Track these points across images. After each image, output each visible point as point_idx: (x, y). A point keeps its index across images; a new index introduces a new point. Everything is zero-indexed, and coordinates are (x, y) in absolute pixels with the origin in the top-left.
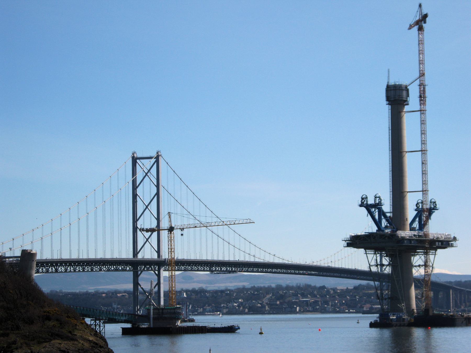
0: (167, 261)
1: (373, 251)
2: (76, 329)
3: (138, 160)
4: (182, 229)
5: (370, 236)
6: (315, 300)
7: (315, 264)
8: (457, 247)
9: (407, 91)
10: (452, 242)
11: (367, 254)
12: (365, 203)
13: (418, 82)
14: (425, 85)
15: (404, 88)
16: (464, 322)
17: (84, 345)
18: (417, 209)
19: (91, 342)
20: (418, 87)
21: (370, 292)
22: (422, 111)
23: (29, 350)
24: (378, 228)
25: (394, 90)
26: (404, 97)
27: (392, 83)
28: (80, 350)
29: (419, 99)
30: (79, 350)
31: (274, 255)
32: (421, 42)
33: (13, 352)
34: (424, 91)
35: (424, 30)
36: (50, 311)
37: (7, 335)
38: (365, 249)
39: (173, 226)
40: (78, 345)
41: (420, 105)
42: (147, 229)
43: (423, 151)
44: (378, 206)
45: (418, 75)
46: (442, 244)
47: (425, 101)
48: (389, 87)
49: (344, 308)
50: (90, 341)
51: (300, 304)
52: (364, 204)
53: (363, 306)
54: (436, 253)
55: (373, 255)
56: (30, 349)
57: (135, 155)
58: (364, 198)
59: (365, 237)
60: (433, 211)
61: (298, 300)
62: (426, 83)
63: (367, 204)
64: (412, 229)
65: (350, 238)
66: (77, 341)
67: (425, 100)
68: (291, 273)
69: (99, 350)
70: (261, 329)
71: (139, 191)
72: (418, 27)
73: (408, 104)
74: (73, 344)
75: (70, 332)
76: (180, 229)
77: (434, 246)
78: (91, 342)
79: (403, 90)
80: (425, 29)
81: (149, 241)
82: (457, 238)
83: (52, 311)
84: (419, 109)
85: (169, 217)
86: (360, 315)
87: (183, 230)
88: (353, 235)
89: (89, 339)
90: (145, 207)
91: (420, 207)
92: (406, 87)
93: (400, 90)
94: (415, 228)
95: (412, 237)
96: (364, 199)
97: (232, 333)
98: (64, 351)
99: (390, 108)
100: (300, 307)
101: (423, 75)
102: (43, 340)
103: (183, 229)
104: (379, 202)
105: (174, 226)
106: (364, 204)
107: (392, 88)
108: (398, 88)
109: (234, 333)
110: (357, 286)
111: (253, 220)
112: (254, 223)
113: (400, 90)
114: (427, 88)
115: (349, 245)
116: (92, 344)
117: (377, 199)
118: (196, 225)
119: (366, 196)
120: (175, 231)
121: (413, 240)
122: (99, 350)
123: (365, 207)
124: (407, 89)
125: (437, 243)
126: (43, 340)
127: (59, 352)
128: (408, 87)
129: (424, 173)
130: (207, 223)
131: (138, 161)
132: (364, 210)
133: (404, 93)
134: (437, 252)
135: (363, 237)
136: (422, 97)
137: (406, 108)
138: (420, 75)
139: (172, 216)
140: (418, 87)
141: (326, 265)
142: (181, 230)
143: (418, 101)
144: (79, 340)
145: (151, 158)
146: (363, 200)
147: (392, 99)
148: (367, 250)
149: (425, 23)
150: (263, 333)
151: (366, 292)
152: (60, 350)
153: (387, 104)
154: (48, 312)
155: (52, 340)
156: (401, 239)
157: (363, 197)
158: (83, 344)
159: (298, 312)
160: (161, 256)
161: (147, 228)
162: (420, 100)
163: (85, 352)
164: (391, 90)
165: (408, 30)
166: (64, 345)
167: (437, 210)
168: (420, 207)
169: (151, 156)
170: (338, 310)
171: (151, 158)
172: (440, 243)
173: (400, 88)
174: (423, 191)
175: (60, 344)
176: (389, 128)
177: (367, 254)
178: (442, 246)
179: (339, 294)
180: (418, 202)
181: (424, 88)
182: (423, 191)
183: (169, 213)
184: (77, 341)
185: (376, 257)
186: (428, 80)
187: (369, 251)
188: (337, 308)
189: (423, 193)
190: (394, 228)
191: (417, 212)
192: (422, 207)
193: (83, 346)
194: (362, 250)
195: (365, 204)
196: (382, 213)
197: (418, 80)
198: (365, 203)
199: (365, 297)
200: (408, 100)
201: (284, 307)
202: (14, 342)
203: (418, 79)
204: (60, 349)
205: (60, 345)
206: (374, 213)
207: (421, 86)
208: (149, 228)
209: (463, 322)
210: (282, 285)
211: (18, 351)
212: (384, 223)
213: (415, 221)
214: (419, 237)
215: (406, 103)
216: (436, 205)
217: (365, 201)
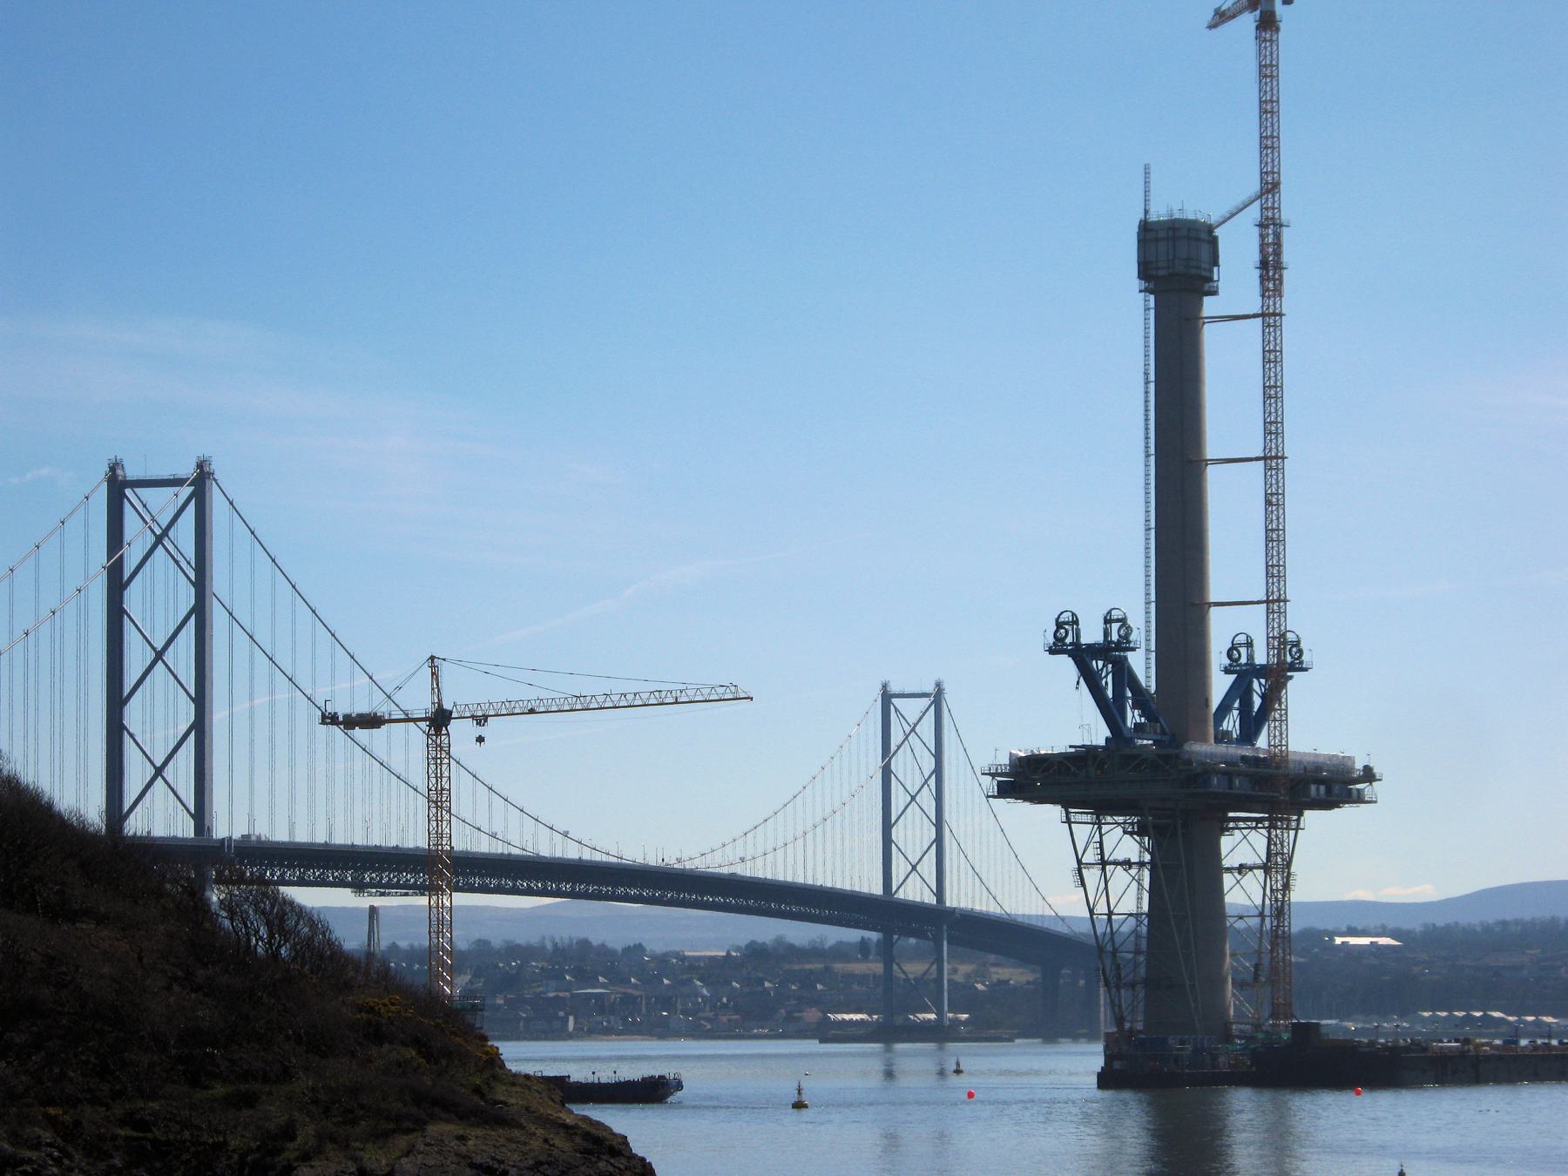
0: (230, 846)
1: (1078, 813)
2: (494, 1077)
3: (130, 490)
4: (481, 720)
5: (1083, 757)
6: (625, 993)
7: (689, 866)
8: (1376, 802)
9: (1213, 242)
11: (1072, 825)
12: (1069, 640)
13: (1254, 212)
14: (1281, 226)
15: (1204, 236)
17: (553, 1145)
18: (1230, 665)
19: (570, 1131)
20: (1255, 232)
21: (808, 966)
22: (1270, 317)
23: (350, 1163)
24: (1111, 732)
26: (1203, 266)
27: (1159, 213)
28: (541, 1163)
29: (1258, 273)
30: (539, 1163)
31: (565, 834)
32: (1267, 72)
33: (295, 1172)
34: (1278, 244)
35: (1278, 30)
36: (378, 1004)
37: (249, 1100)
38: (1066, 805)
39: (447, 706)
40: (530, 1144)
41: (1263, 296)
42: (347, 717)
43: (1272, 460)
44: (1113, 651)
45: (1254, 187)
46: (1329, 791)
47: (1281, 283)
48: (1152, 230)
49: (729, 1020)
50: (566, 1127)
51: (580, 1007)
52: (1065, 644)
53: (796, 1014)
54: (1302, 826)
56: (355, 1159)
57: (119, 472)
58: (1067, 623)
59: (1066, 762)
60: (1289, 674)
61: (568, 993)
63: (1076, 644)
64: (1220, 737)
65: (1010, 765)
66: (520, 1127)
67: (1281, 276)
68: (626, 898)
69: (615, 1167)
71: (133, 599)
72: (1258, 19)
73: (1214, 293)
74: (510, 1140)
75: (477, 1090)
76: (473, 717)
77: (1304, 799)
78: (576, 1134)
80: (1282, 26)
81: (165, 775)
83: (385, 1005)
84: (1257, 309)
85: (433, 674)
86: (812, 1046)
87: (486, 721)
88: (1022, 754)
89: (561, 1122)
90: (153, 654)
91: (1243, 660)
92: (1210, 229)
94: (1228, 733)
96: (1066, 625)
97: (655, 1106)
98: (489, 1170)
99: (1152, 304)
101: (1276, 185)
102: (391, 1126)
103: (486, 717)
104: (1119, 636)
105: (450, 708)
106: (1065, 641)
107: (1162, 234)
109: (663, 1106)
110: (619, 947)
111: (745, 688)
112: (752, 699)
114: (1286, 234)
115: (1005, 791)
116: (578, 1139)
117: (1115, 626)
118: (533, 704)
119: (1073, 614)
120: (454, 726)
121: (1239, 774)
122: (615, 1167)
123: (1071, 654)
124: (1211, 239)
125: (1313, 788)
126: (391, 1126)
127: (468, 1171)
128: (1217, 232)
130: (575, 699)
131: (128, 492)
132: (1066, 664)
133: (1205, 249)
134: (1302, 818)
135: (1060, 763)
136: (1270, 267)
137: (1210, 306)
138: (1262, 188)
139: (445, 670)
140: (1256, 231)
141: (725, 871)
142: (475, 722)
143: (1257, 281)
144: (525, 1124)
145: (176, 482)
146: (1062, 631)
147: (1161, 273)
148: (1070, 810)
150: (806, 1106)
151: (797, 967)
152: (472, 1166)
153: (1140, 291)
154: (371, 1010)
155: (425, 1123)
156: (1199, 770)
157: (1061, 620)
158: (546, 1141)
159: (571, 1033)
160: (206, 829)
161: (348, 711)
162: (1264, 279)
163: (563, 1172)
164: (1157, 240)
165: (1208, 30)
166: (481, 1143)
167: (1306, 670)
168: (1243, 660)
169: (176, 477)
170: (709, 1027)
171: (176, 482)
172: (1322, 788)
174: (1267, 602)
175: (462, 1138)
176: (1146, 374)
177: (1072, 825)
178: (1330, 798)
179: (701, 971)
180: (1237, 640)
181: (1278, 236)
182: (1267, 602)
183: (432, 658)
184: (520, 1127)
185: (1101, 836)
186: (1290, 205)
187: (1078, 815)
188: (703, 1022)
189: (1268, 609)
190: (1163, 732)
191: (1233, 677)
192: (1248, 660)
193: (547, 1147)
194: (1054, 812)
195: (1071, 644)
196: (1124, 675)
197: (1257, 204)
198: (1069, 640)
199: (795, 985)
200: (1215, 278)
201: (524, 1015)
202: (288, 1133)
203: (1257, 199)
204: (470, 1161)
205: (464, 1142)
206: (1103, 675)
207: (1267, 227)
208: (357, 715)
210: (585, 944)
211: (312, 1167)
212: (1133, 717)
213: (1231, 710)
215: (1206, 287)
216: (1300, 651)
217: (1070, 633)
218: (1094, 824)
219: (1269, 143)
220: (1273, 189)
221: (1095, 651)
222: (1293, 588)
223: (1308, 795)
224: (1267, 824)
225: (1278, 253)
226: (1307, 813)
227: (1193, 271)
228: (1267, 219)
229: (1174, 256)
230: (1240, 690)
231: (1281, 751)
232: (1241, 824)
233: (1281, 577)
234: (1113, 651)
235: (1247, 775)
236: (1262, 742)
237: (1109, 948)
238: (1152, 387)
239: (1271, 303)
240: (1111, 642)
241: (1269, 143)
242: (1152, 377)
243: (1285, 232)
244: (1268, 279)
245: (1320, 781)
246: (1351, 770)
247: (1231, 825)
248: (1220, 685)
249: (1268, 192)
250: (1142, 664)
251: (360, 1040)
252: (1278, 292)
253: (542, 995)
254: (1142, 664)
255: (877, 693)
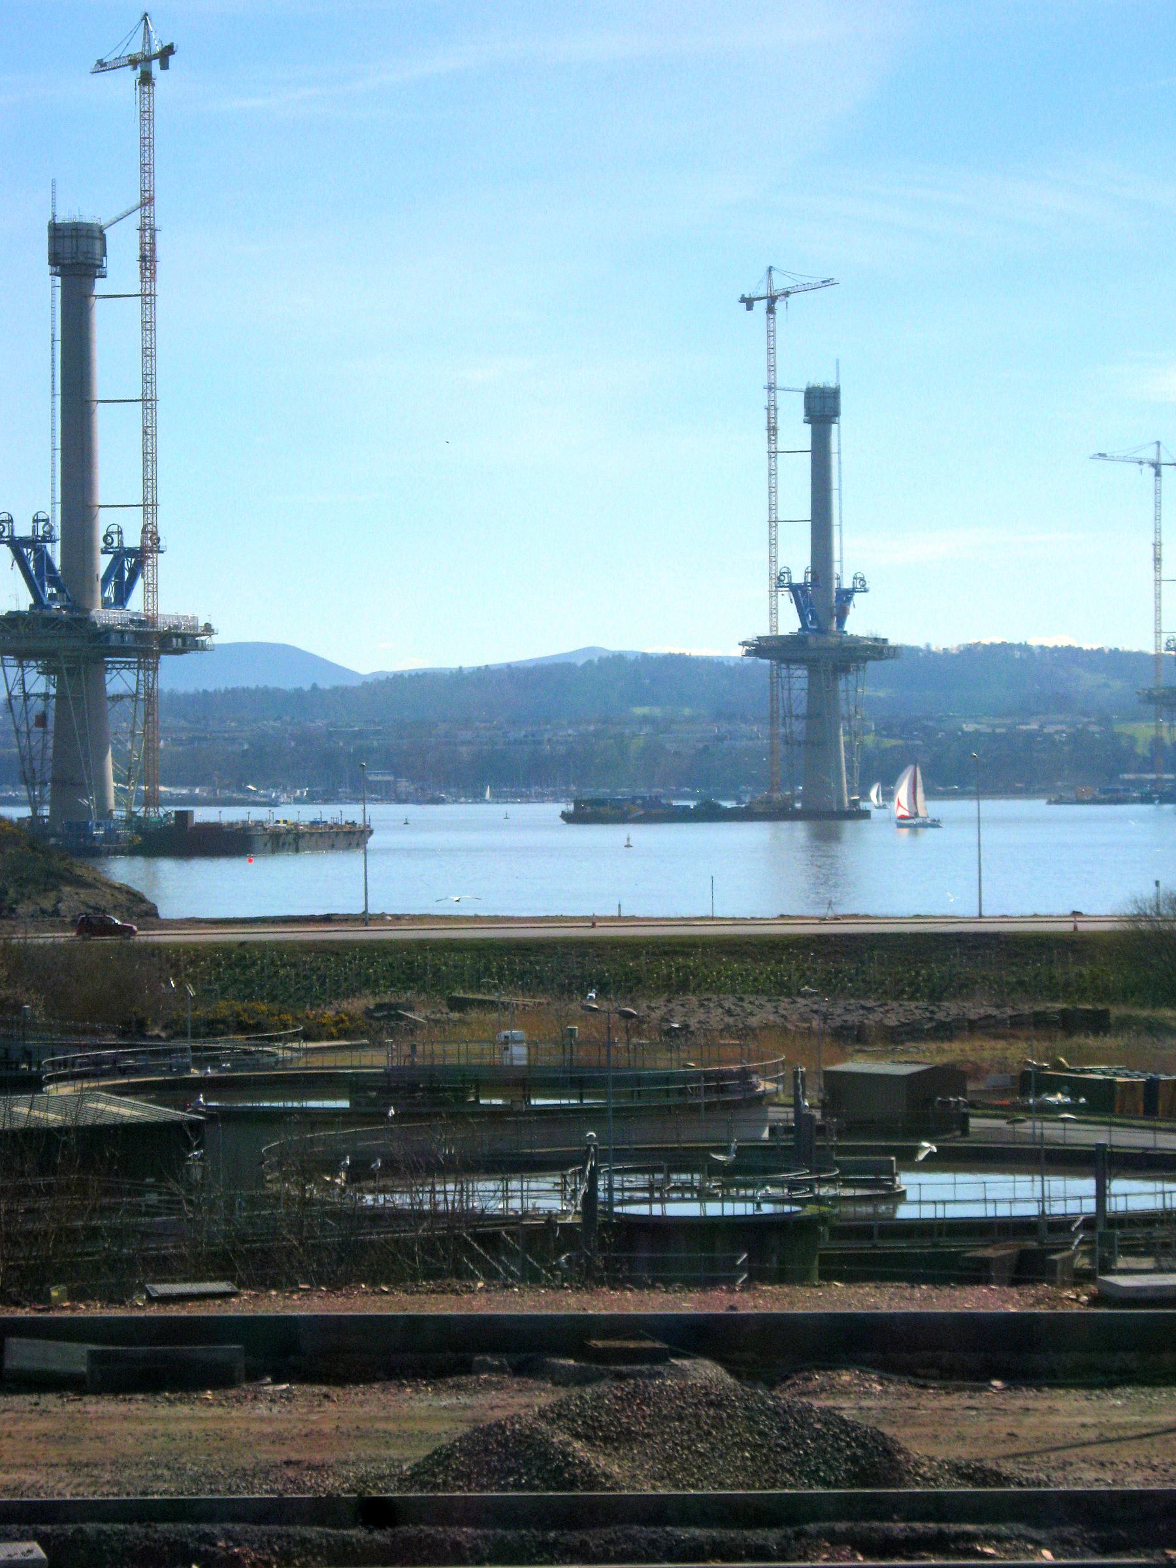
9: (103, 239)
10: (203, 638)
13: (135, 219)
14: (155, 230)
15: (97, 234)
16: (269, 845)
22: (147, 297)
25: (72, 237)
27: (63, 217)
34: (153, 244)
35: (153, 85)
41: (142, 281)
43: (148, 401)
45: (137, 200)
47: (155, 272)
48: (59, 230)
55: (16, 669)
62: (157, 225)
63: (12, 537)
67: (155, 266)
70: (628, 839)
79: (94, 238)
82: (214, 627)
91: (115, 544)
93: (88, 237)
94: (109, 599)
95: (126, 625)
100: (883, 785)
104: (44, 532)
108: (84, 233)
113: (88, 237)
117: (41, 524)
125: (174, 640)
128: (106, 232)
129: (149, 457)
133: (98, 244)
136: (148, 260)
147: (66, 262)
149: (165, 66)
156: (102, 630)
162: (143, 269)
164: (64, 237)
168: (115, 544)
173: (90, 234)
180: (110, 530)
181: (153, 237)
196: (43, 559)
207: (145, 230)
209: (266, 845)
214: (139, 626)
216: (159, 539)
218: (18, 666)
219: (147, 169)
220: (149, 202)
221: (25, 542)
222: (164, 496)
223: (171, 646)
224: (136, 665)
225: (153, 250)
226: (162, 656)
227: (90, 261)
228: (145, 225)
229: (77, 247)
230: (115, 568)
231: (153, 614)
232: (117, 666)
233: (154, 488)
234: (36, 543)
235: (133, 632)
236: (136, 603)
237: (28, 757)
238: (58, 346)
239: (148, 287)
240: (38, 536)
241: (147, 169)
242: (58, 336)
243: (158, 235)
244: (146, 269)
245: (178, 636)
246: (195, 627)
247: (110, 666)
248: (103, 562)
249: (145, 205)
250: (55, 552)
251: (646, 1431)
252: (153, 278)
253: (837, 1412)
254: (55, 552)
255: (765, 269)
